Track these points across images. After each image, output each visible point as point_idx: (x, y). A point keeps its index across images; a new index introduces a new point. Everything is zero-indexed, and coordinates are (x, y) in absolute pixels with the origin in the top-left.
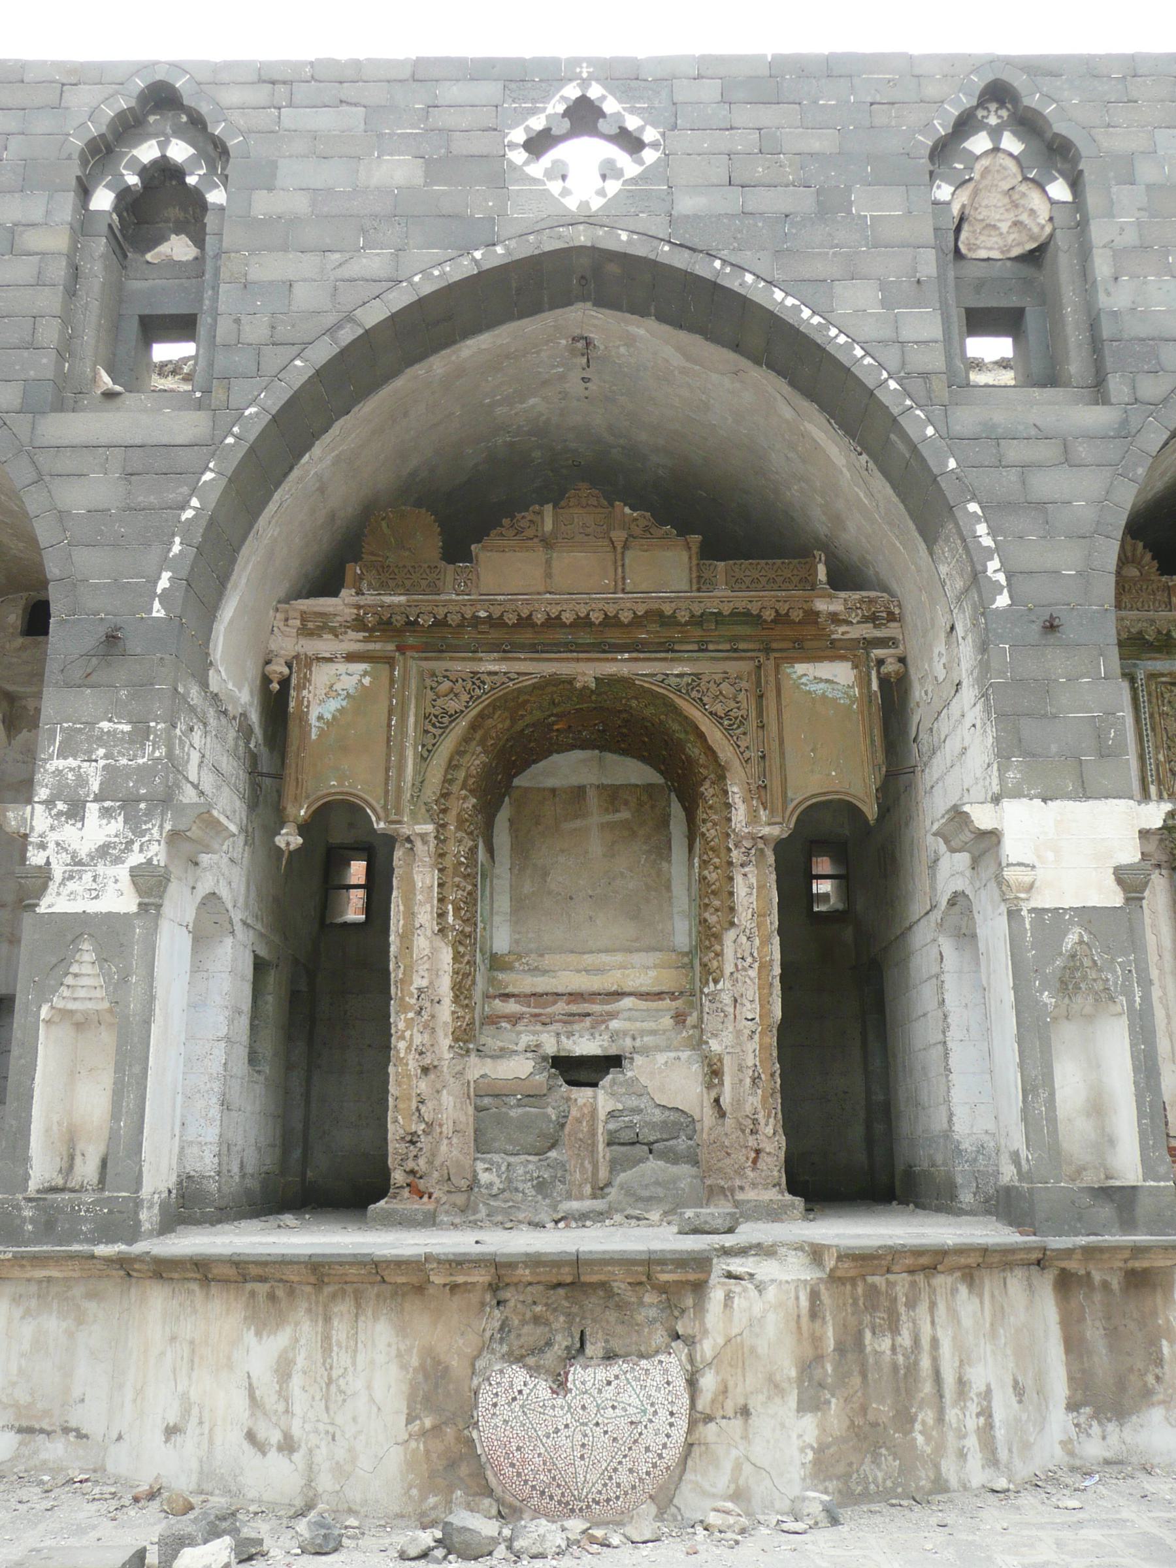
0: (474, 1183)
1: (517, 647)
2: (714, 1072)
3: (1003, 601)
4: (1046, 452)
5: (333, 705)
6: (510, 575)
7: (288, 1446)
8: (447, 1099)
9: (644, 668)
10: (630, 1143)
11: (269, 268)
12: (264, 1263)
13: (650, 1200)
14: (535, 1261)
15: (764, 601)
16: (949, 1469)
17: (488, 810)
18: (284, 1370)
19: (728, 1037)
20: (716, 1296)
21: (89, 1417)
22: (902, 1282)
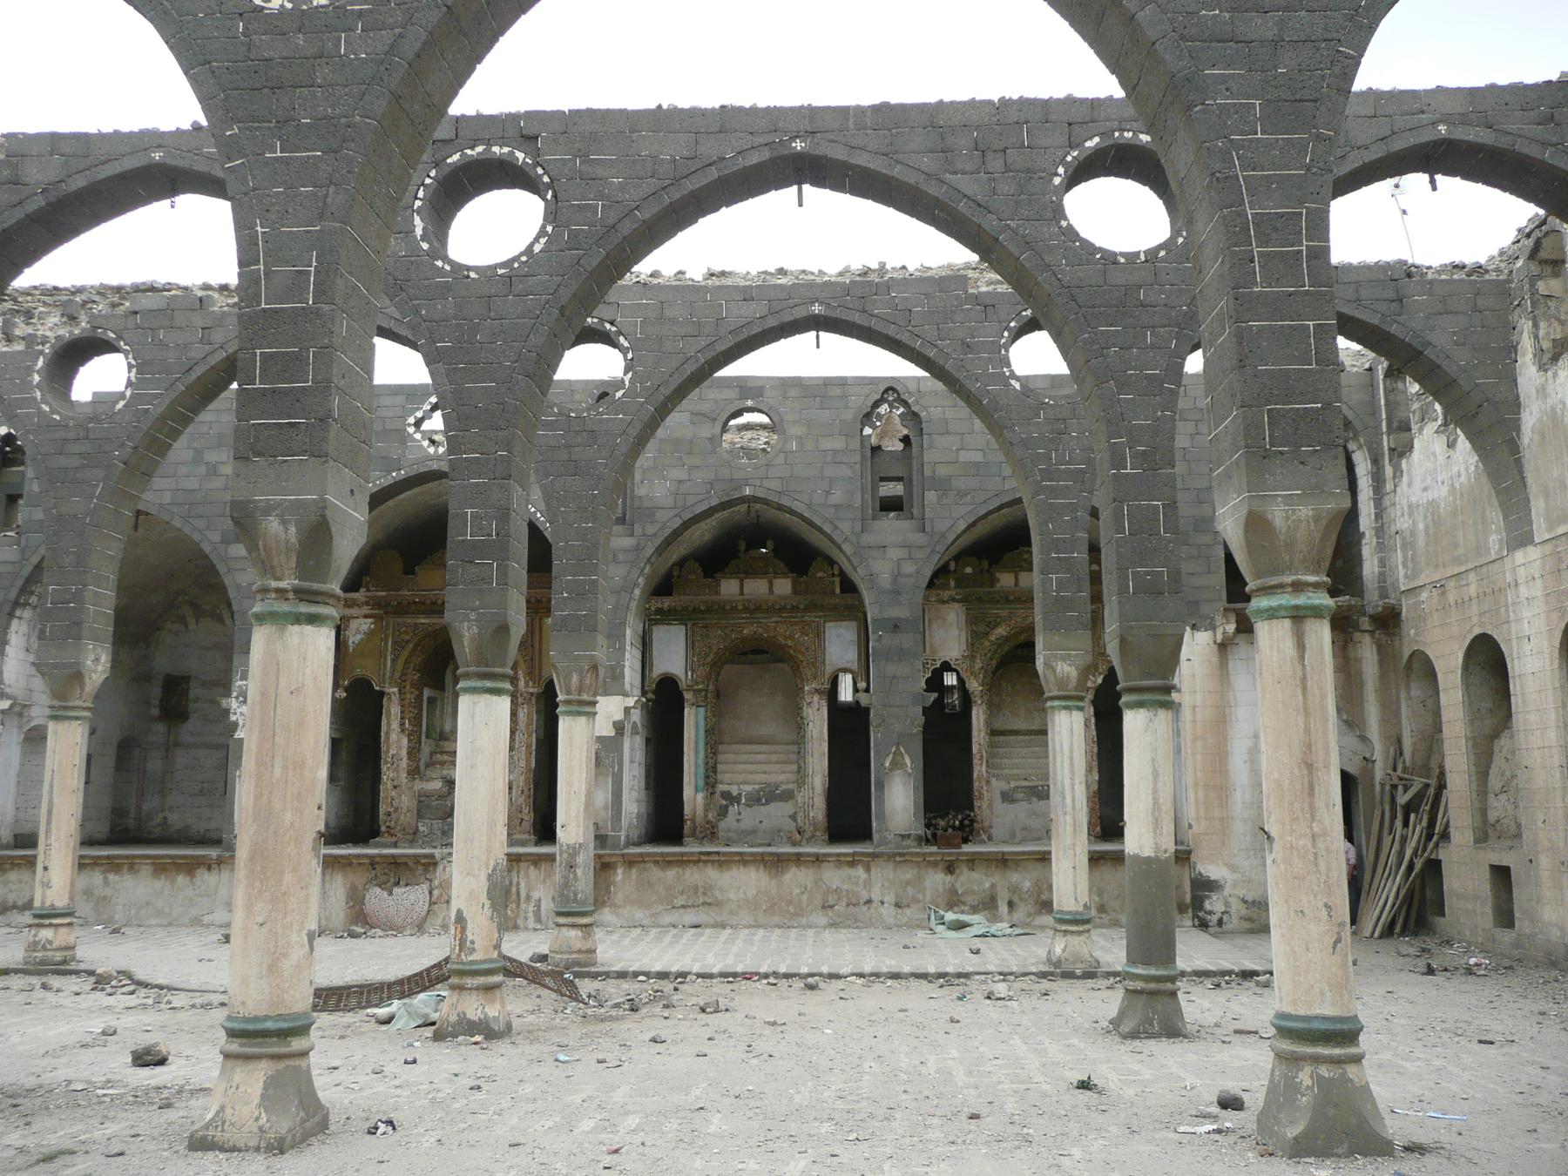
0: (416, 832)
5: (359, 637)
16: (520, 922)
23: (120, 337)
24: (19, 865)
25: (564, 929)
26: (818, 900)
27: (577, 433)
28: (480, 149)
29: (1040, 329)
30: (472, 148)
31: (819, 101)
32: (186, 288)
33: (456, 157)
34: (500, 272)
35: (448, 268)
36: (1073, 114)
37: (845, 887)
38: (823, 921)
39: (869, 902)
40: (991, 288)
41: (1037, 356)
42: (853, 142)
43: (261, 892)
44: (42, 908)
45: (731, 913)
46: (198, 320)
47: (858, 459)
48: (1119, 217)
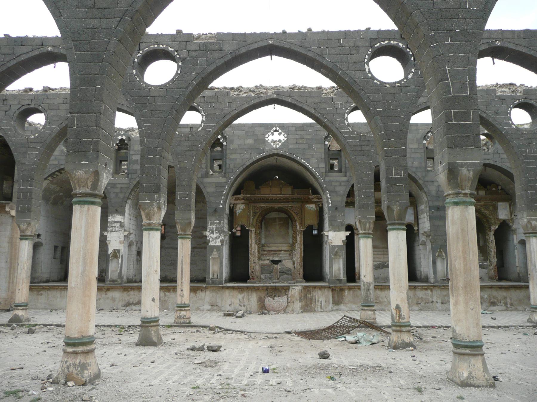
0: (261, 278)
1: (267, 202)
2: (294, 263)
3: (330, 205)
4: (337, 184)
5: (240, 211)
6: (266, 192)
7: (244, 306)
8: (257, 267)
9: (285, 206)
10: (282, 272)
11: (233, 156)
12: (241, 286)
13: (285, 280)
14: (271, 286)
15: (302, 196)
16: (316, 309)
17: (261, 222)
18: (243, 298)
19: (296, 258)
20: (290, 290)
21: (219, 304)
22: (311, 289)
23: (198, 105)
24: (134, 289)
25: (367, 311)
26: (415, 302)
27: (364, 141)
28: (386, 42)
29: (358, 109)
30: (384, 42)
31: (504, 28)
32: (218, 89)
33: (378, 45)
34: (397, 85)
35: (379, 83)
36: (381, 34)
37: (424, 297)
38: (417, 308)
39: (433, 302)
40: (502, 93)
41: (357, 117)
42: (517, 43)
43: (471, 298)
44: (181, 304)
45: (385, 306)
46: (227, 100)
47: (423, 151)
48: (387, 70)
